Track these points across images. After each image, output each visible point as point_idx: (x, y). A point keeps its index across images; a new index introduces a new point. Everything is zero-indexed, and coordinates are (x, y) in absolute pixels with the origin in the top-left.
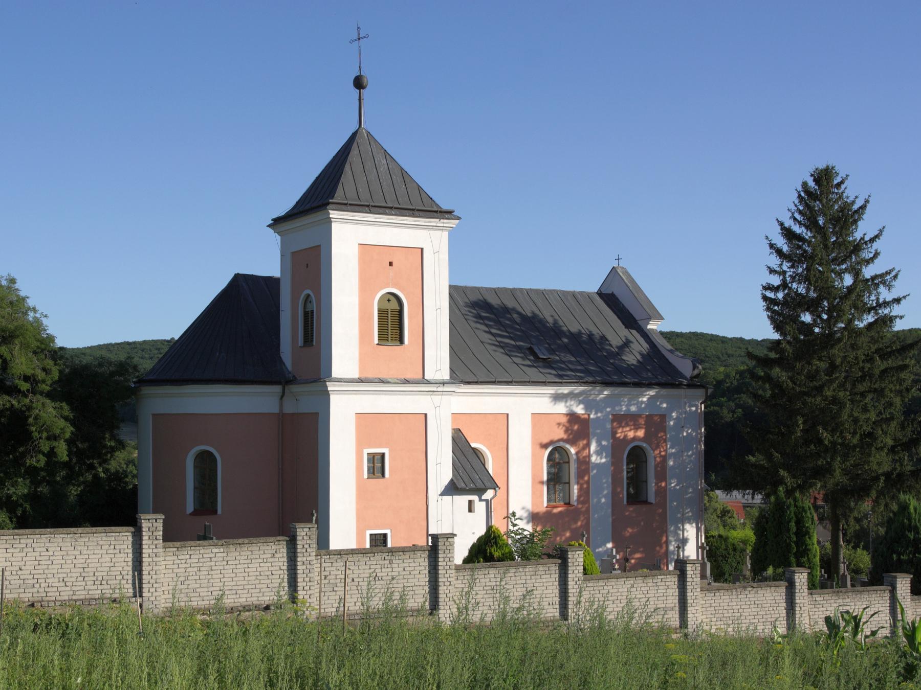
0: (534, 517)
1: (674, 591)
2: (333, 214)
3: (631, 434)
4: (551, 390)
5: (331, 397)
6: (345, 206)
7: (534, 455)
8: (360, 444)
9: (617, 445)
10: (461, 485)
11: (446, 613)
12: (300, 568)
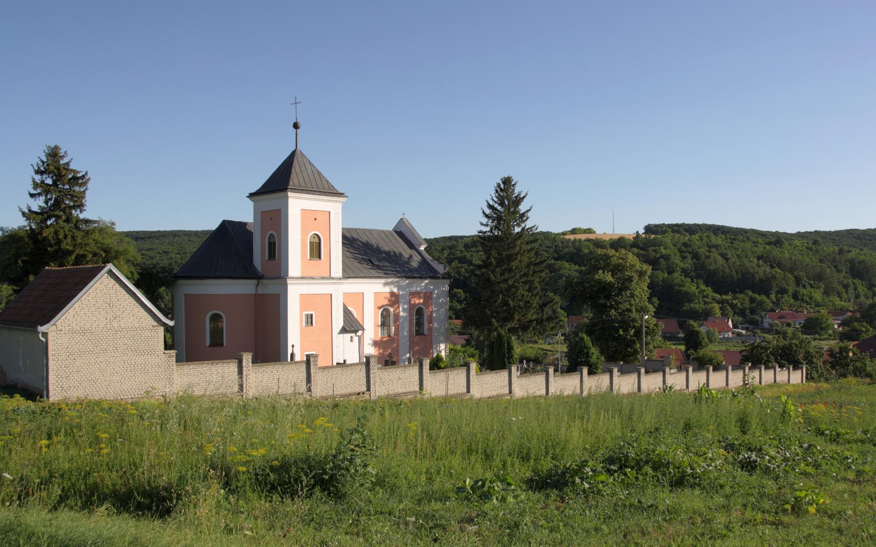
0: (376, 344)
1: (507, 378)
2: (290, 194)
3: (417, 302)
4: (383, 281)
5: (289, 287)
6: (295, 190)
7: (375, 313)
8: (302, 309)
9: (411, 306)
10: (348, 329)
11: (585, 394)
12: (372, 375)
